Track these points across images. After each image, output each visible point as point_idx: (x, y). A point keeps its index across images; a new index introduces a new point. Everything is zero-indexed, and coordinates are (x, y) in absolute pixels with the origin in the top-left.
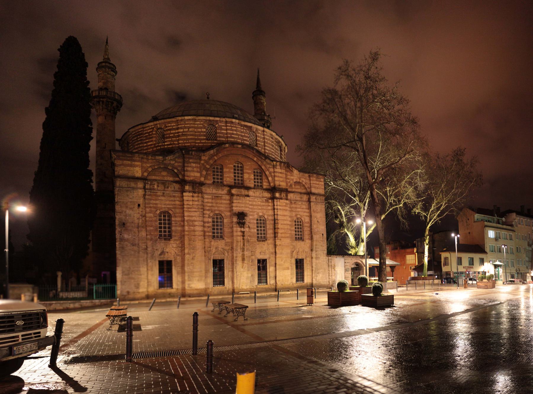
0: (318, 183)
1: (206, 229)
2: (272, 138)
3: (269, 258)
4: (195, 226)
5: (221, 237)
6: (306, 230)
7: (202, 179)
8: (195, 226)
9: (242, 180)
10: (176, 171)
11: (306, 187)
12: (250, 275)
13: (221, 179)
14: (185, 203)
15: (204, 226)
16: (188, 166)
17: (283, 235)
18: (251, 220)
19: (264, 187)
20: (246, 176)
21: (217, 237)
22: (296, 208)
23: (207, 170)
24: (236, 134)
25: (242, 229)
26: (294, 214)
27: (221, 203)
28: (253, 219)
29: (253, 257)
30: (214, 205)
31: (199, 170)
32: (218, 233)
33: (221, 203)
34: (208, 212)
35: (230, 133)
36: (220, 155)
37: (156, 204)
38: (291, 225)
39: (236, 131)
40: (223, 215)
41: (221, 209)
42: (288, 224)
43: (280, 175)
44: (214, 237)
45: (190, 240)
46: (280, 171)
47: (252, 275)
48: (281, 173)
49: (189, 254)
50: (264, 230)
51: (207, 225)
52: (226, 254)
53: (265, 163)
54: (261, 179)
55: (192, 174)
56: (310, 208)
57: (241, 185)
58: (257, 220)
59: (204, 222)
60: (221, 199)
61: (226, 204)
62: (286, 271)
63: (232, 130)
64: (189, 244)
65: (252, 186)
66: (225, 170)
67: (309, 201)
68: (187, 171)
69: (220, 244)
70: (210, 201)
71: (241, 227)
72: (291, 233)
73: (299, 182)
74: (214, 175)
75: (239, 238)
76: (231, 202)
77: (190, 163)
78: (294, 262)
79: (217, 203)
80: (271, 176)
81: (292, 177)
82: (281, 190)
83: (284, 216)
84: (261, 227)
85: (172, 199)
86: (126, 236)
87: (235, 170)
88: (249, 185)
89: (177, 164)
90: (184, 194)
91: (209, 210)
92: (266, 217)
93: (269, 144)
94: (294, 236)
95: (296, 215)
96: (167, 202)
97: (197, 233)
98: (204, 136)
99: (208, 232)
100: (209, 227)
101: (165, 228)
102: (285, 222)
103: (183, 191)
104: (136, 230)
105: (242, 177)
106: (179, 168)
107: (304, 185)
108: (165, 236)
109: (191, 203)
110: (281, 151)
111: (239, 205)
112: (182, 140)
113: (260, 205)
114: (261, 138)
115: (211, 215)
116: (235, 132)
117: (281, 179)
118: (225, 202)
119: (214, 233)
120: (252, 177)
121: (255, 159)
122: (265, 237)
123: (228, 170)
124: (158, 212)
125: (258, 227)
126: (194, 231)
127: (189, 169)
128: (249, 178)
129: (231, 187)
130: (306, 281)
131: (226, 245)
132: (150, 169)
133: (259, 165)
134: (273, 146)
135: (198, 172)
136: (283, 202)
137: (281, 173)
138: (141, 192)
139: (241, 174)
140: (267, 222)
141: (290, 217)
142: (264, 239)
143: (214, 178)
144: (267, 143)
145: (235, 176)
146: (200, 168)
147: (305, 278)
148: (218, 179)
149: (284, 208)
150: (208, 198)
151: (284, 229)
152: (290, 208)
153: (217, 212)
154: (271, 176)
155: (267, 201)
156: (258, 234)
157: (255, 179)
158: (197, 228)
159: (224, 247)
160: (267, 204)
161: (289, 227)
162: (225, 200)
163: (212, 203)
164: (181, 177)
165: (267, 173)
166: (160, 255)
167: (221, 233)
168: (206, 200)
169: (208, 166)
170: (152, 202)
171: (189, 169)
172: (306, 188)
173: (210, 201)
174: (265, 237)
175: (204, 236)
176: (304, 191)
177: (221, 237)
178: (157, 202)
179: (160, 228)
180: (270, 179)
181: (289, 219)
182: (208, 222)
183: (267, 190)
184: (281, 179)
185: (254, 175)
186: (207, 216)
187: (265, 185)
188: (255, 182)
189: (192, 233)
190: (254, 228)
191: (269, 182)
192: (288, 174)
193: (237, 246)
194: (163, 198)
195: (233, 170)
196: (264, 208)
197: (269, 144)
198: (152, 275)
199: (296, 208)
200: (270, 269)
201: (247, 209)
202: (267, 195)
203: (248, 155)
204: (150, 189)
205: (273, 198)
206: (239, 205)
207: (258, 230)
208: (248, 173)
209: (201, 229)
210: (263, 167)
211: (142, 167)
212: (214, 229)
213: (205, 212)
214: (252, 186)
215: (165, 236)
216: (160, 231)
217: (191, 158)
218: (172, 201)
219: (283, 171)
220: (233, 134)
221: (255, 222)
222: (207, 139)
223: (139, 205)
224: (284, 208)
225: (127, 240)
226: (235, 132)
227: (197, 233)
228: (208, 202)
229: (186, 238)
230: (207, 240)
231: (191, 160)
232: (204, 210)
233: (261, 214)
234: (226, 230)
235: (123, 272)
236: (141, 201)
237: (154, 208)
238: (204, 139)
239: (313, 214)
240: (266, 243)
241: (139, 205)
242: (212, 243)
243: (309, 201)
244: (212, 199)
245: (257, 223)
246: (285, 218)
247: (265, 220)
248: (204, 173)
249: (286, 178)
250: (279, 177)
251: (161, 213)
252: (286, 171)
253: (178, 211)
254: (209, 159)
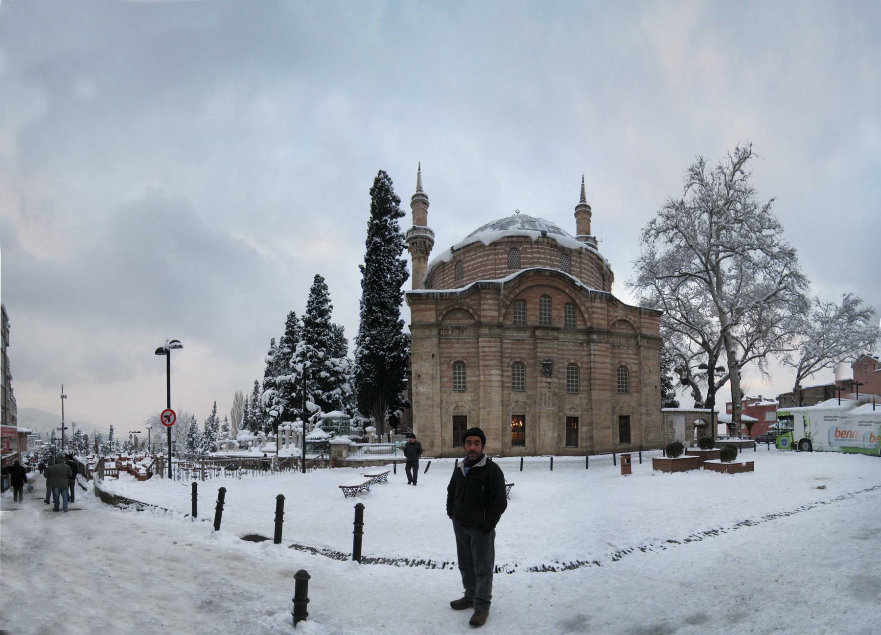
0: (651, 321)
1: (504, 379)
2: (592, 263)
3: (582, 416)
4: (491, 375)
5: (626, 391)
6: (633, 381)
7: (501, 319)
8: (491, 375)
9: (549, 319)
10: (471, 311)
11: (635, 326)
12: (556, 435)
13: (524, 318)
14: (481, 350)
15: (502, 376)
16: (484, 304)
17: (596, 353)
18: (560, 368)
19: (579, 327)
20: (554, 313)
21: (518, 388)
22: (620, 353)
23: (507, 307)
24: (544, 258)
25: (549, 380)
26: (617, 361)
27: (523, 349)
28: (563, 368)
29: (561, 414)
30: (514, 351)
31: (497, 307)
32: (518, 383)
33: (523, 349)
34: (507, 360)
35: (536, 258)
36: (523, 287)
37: (450, 353)
38: (612, 375)
39: (543, 253)
40: (525, 363)
41: (522, 356)
42: (608, 374)
43: (600, 311)
44: (514, 388)
45: (485, 392)
46: (600, 305)
47: (559, 436)
48: (601, 308)
49: (484, 408)
50: (576, 382)
51: (506, 374)
52: (528, 409)
53: (580, 295)
54: (574, 317)
55: (489, 313)
56: (638, 354)
57: (547, 327)
58: (568, 368)
59: (503, 371)
60: (523, 344)
61: (529, 349)
62: (607, 431)
63: (539, 253)
64: (485, 397)
65: (562, 326)
66: (528, 306)
67: (638, 347)
68: (483, 310)
69: (521, 397)
70: (510, 346)
71: (547, 377)
72: (611, 386)
73: (625, 321)
74: (515, 313)
75: (544, 390)
76: (535, 346)
77: (487, 299)
78: (616, 418)
79: (518, 349)
80: (588, 312)
81: (616, 314)
82: (600, 332)
83: (604, 363)
84: (572, 377)
85: (467, 345)
86: (421, 389)
87: (541, 305)
88: (558, 325)
89: (472, 302)
90: (480, 339)
91: (508, 358)
92: (579, 365)
93: (588, 270)
94: (617, 389)
95: (620, 362)
96: (462, 350)
97: (493, 384)
98: (505, 263)
99: (508, 382)
100: (508, 376)
101: (459, 378)
102: (605, 371)
103: (478, 336)
104: (429, 382)
105: (549, 315)
106: (475, 307)
107: (631, 325)
108: (460, 387)
109: (487, 350)
110: (604, 280)
111: (544, 350)
112: (480, 272)
113: (572, 350)
114: (576, 262)
115: (511, 363)
116: (542, 256)
117: (602, 317)
118: (527, 347)
119: (514, 383)
120: (563, 314)
121: (567, 291)
122: (577, 390)
123: (532, 306)
124: (452, 362)
125: (568, 377)
126: (491, 381)
127: (486, 307)
128: (558, 316)
129: (536, 328)
130: (632, 441)
131: (528, 398)
132: (444, 312)
133: (572, 299)
134: (592, 273)
135: (495, 310)
136: (603, 346)
137: (601, 308)
138: (435, 340)
139: (549, 310)
140: (581, 371)
141: (611, 365)
142: (577, 392)
143: (515, 318)
144: (585, 269)
145: (541, 314)
146: (498, 304)
147: (632, 438)
148: (519, 318)
149: (603, 353)
150: (507, 343)
151: (603, 379)
152: (612, 353)
153: (518, 360)
154: (588, 312)
155: (581, 344)
156: (568, 386)
157: (566, 316)
158: (494, 378)
159: (525, 400)
160: (580, 348)
161: (609, 377)
162: (528, 344)
163: (512, 349)
164: (476, 318)
165: (583, 308)
166: (455, 409)
167: (518, 388)
168: (505, 346)
169: (508, 303)
170: (446, 350)
171: (486, 307)
172: (634, 329)
173: (510, 346)
174: (577, 390)
175: (502, 387)
176: (631, 332)
177: (523, 388)
178: (452, 350)
179: (455, 378)
180: (586, 316)
181: (610, 367)
182: (507, 371)
183: (581, 331)
184: (602, 317)
185: (566, 312)
186: (506, 365)
187: (580, 325)
188: (566, 320)
189: (488, 384)
190: (564, 379)
191: (584, 320)
192: (611, 309)
193: (541, 400)
194: (457, 346)
195: (538, 306)
196: (578, 353)
197: (588, 270)
198: (446, 432)
199: (620, 353)
200: (583, 430)
201: (556, 355)
202: (581, 337)
203: (558, 285)
204: (445, 336)
205: (589, 342)
206: (544, 350)
207: (568, 381)
208: (557, 309)
209: (499, 378)
210: (577, 301)
211: (437, 310)
212: (514, 379)
213: (504, 360)
214: (562, 326)
215: (460, 387)
216: (455, 382)
217: (488, 293)
218: (467, 348)
219: (604, 305)
220: (540, 258)
221: (565, 370)
222: (509, 268)
223: (433, 356)
224: (603, 353)
225: (423, 394)
226: (542, 256)
227: (493, 384)
228: (507, 348)
229: (481, 389)
230: (505, 392)
231: (488, 296)
232: (502, 357)
233: (572, 361)
234: (528, 380)
235: (419, 429)
236: (435, 351)
237: (448, 357)
238: (505, 268)
239: (644, 362)
240: (578, 397)
241: (433, 356)
242: (512, 396)
243: (638, 347)
244: (513, 344)
245: (568, 373)
246: (605, 366)
247: (578, 368)
248: (503, 311)
249: (608, 316)
250: (597, 313)
251: (455, 363)
252: (608, 306)
253: (472, 360)
254: (510, 293)
